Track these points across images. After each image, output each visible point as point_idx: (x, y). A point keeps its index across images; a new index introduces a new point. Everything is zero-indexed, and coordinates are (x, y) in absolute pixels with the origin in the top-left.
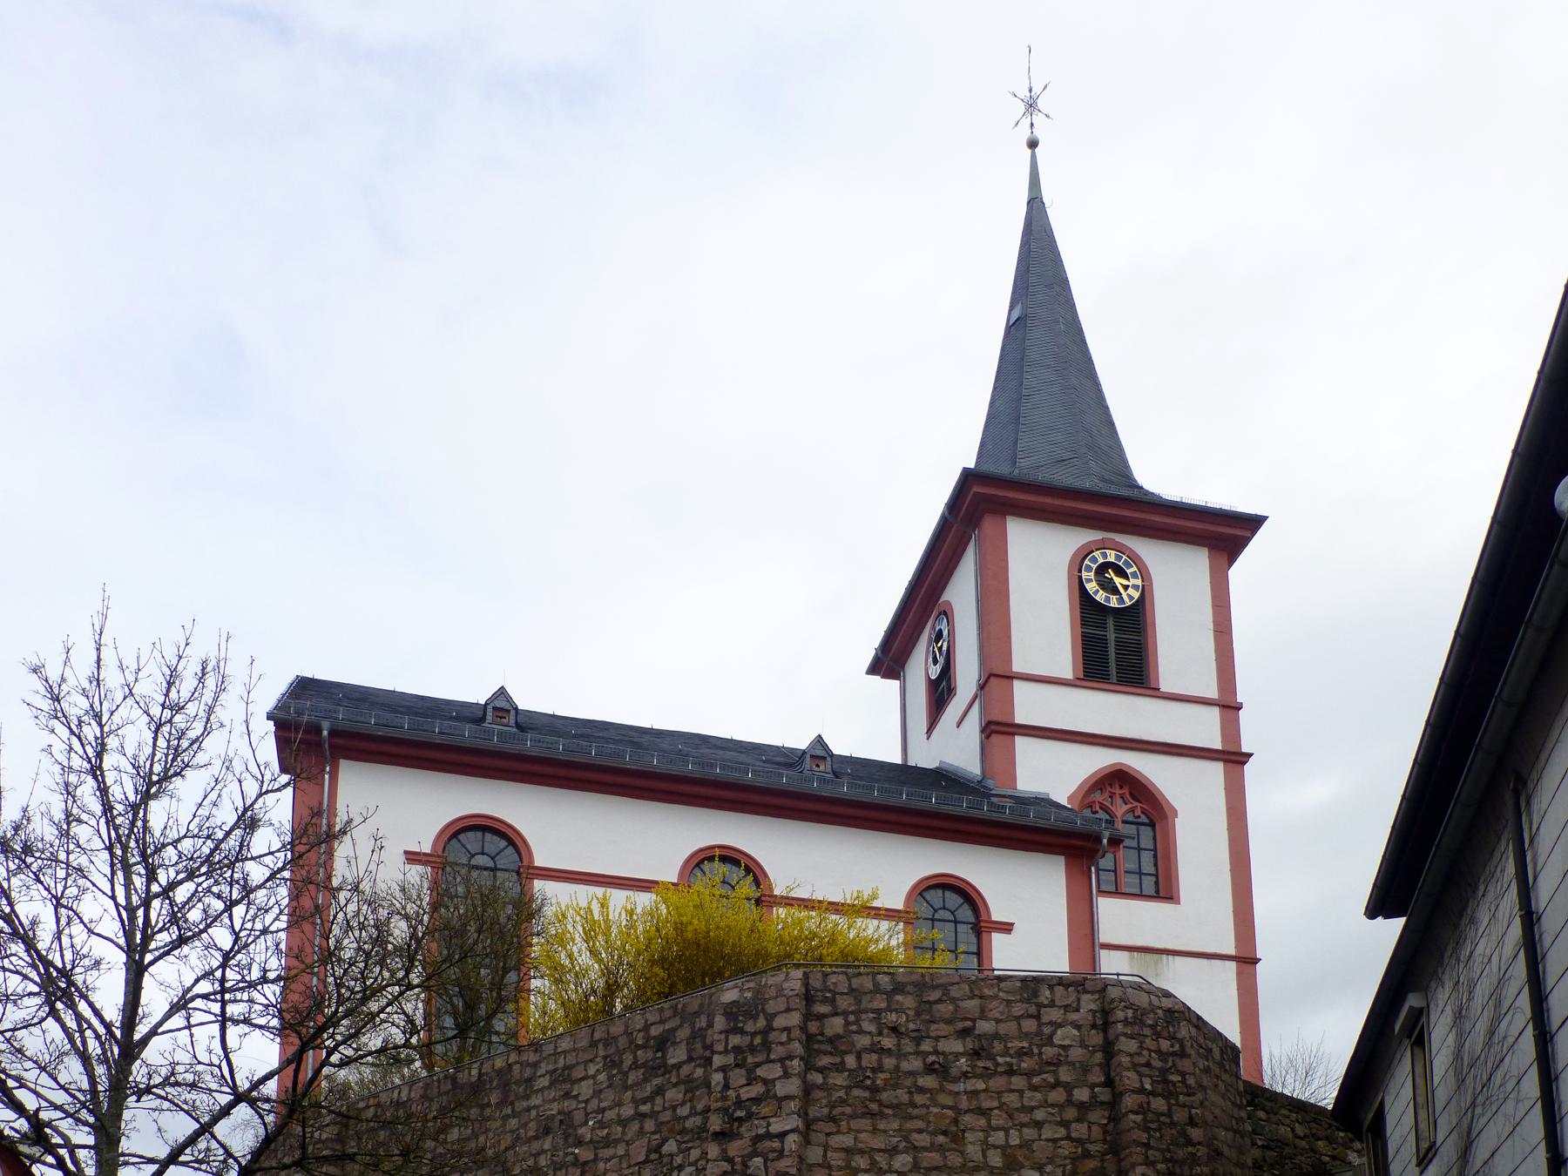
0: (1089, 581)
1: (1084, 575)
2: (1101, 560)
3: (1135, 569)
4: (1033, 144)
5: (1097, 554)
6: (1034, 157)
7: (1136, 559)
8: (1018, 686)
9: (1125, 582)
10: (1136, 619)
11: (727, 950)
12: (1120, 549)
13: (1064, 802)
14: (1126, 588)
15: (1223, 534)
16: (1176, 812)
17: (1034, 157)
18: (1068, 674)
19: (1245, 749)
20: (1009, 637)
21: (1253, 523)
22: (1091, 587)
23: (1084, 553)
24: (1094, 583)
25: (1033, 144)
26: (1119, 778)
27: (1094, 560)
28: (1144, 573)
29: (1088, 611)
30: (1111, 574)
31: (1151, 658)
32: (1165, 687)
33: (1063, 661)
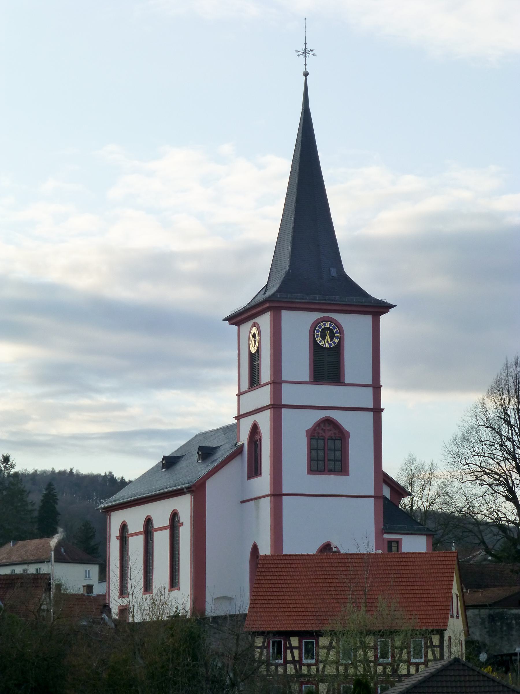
0: (318, 337)
1: (316, 334)
2: (323, 327)
3: (337, 329)
4: (306, 74)
5: (322, 324)
6: (306, 79)
7: (338, 325)
8: (283, 385)
9: (329, 340)
10: (337, 351)
11: (83, 528)
12: (331, 320)
13: (372, 549)
14: (327, 341)
15: (378, 308)
16: (348, 433)
17: (306, 79)
18: (308, 379)
19: (382, 408)
20: (281, 340)
21: (393, 306)
22: (318, 339)
23: (316, 324)
24: (320, 338)
25: (306, 74)
26: (328, 422)
27: (320, 327)
28: (341, 331)
29: (316, 349)
30: (328, 333)
31: (192, 533)
32: (346, 382)
33: (305, 374)
